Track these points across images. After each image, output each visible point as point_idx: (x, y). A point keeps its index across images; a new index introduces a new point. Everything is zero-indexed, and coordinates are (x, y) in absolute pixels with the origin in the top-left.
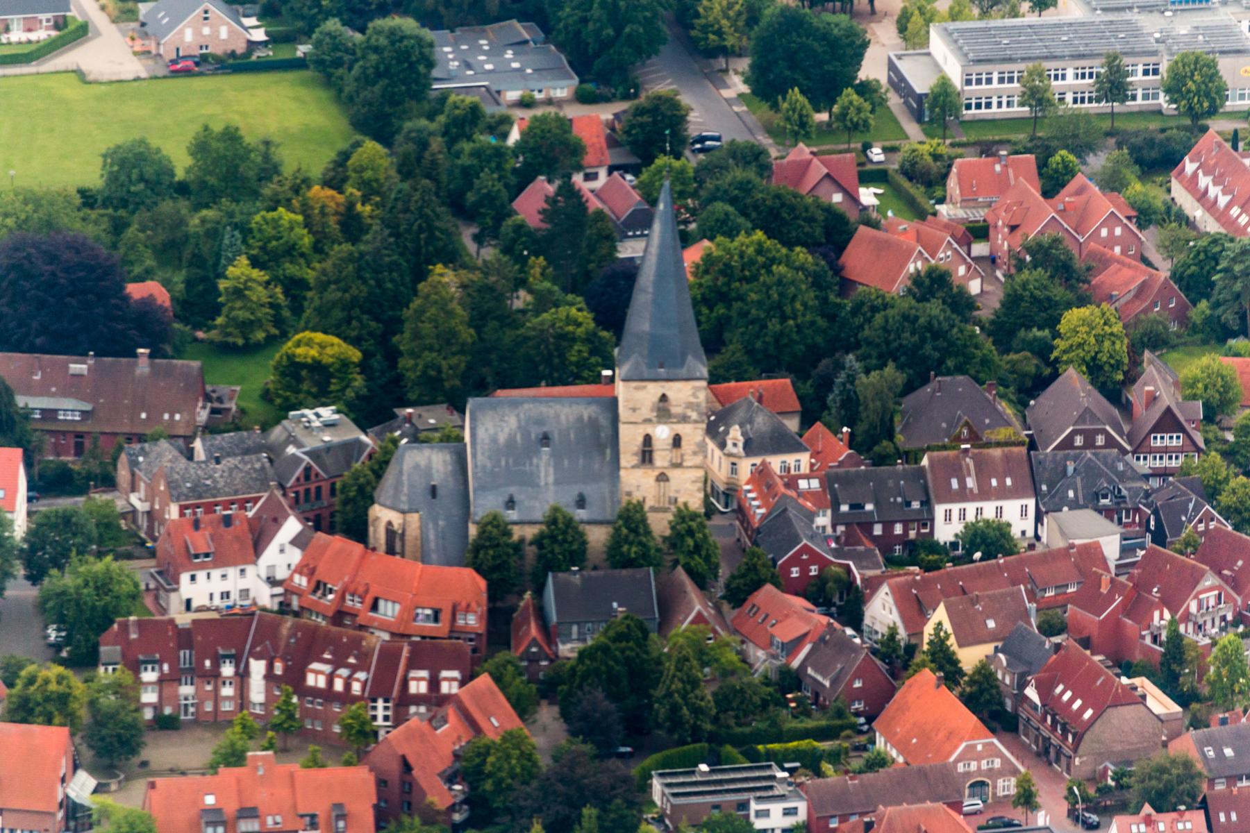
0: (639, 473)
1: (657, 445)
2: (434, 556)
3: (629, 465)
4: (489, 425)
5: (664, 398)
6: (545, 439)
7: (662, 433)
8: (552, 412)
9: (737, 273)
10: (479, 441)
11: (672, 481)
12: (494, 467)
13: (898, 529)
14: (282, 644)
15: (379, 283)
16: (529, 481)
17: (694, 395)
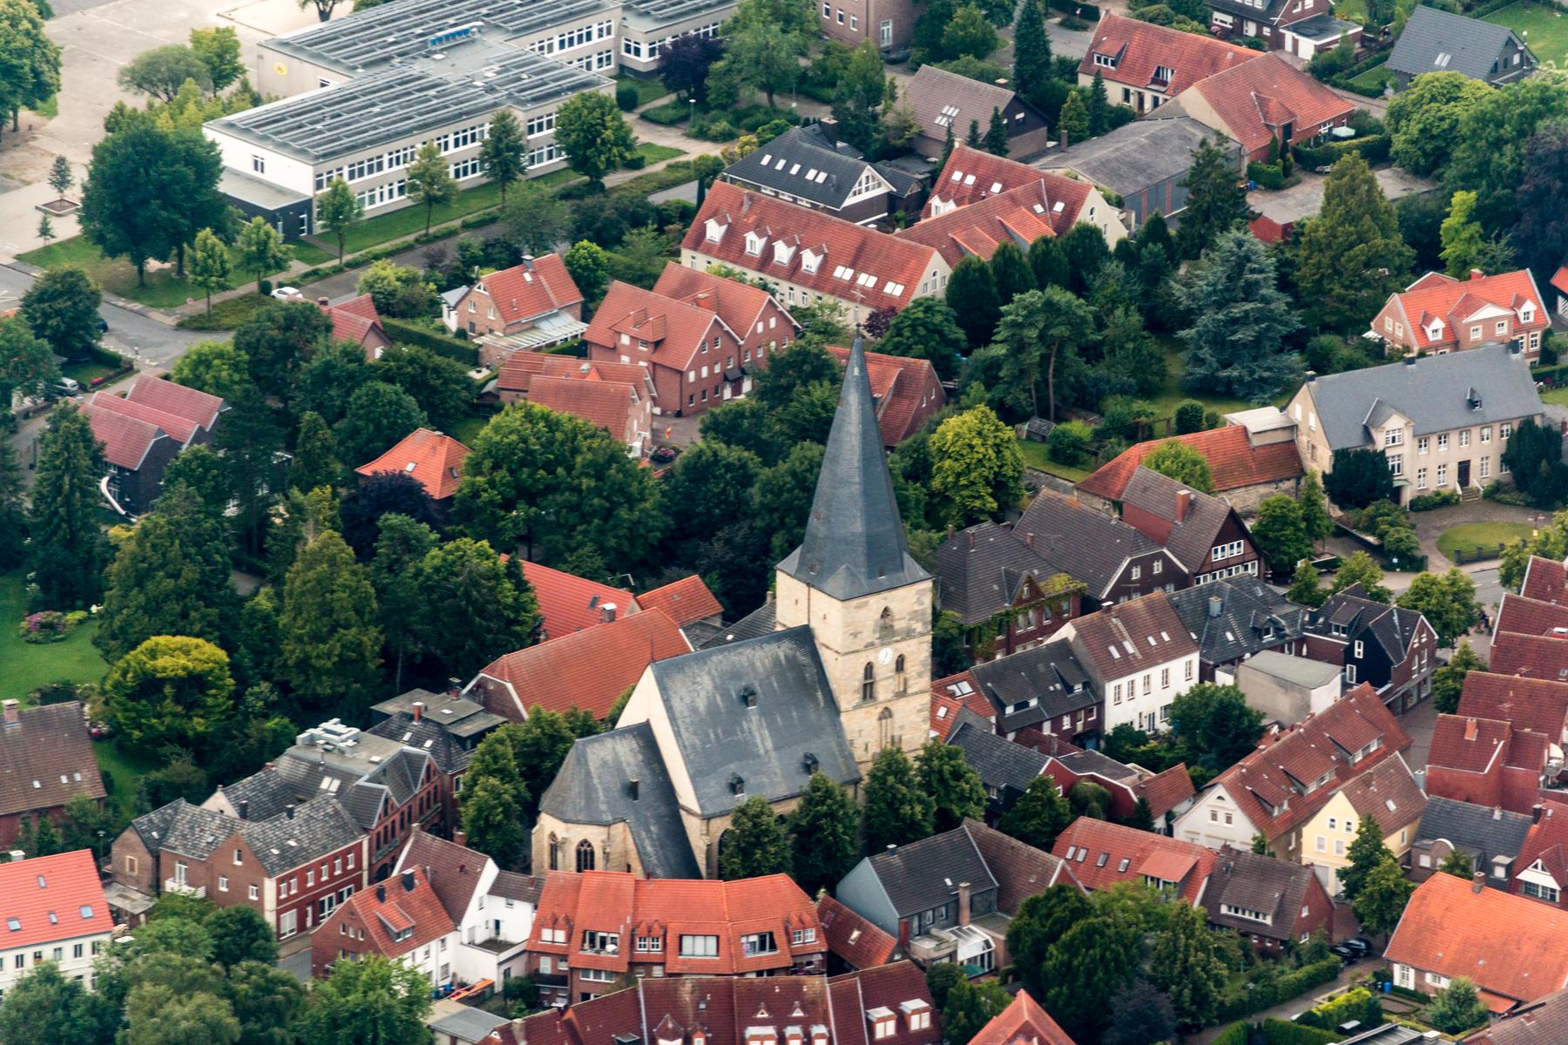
0: (861, 713)
1: (879, 673)
2: (659, 871)
3: (849, 707)
4: (683, 692)
5: (886, 613)
6: (747, 697)
7: (885, 658)
8: (744, 659)
9: (540, 459)
10: (678, 715)
11: (896, 716)
12: (704, 743)
13: (1066, 723)
14: (690, 1012)
15: (208, 560)
16: (745, 751)
17: (919, 602)
